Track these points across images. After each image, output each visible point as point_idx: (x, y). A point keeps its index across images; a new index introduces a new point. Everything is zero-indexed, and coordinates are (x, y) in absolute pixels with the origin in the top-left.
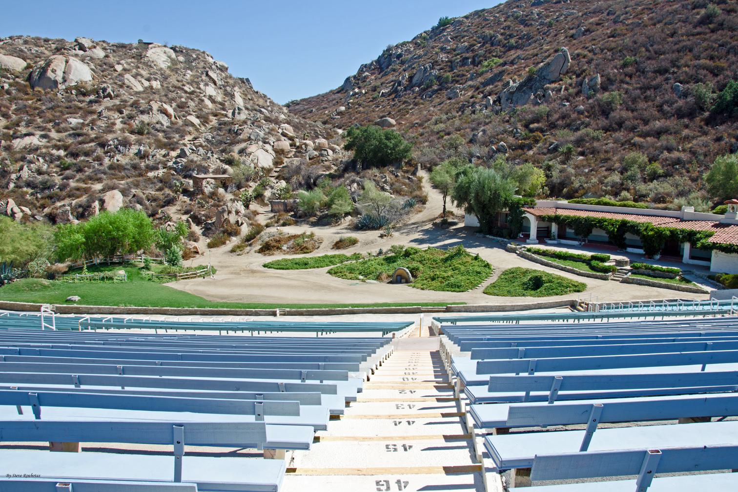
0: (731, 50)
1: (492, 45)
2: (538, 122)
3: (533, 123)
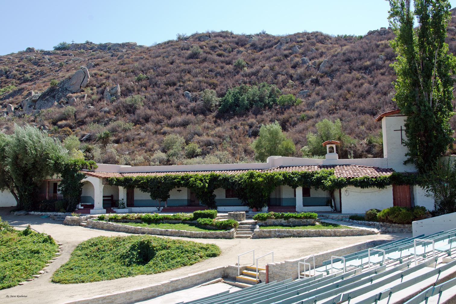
0: (217, 75)
1: (7, 77)
2: (66, 119)
3: (61, 120)
